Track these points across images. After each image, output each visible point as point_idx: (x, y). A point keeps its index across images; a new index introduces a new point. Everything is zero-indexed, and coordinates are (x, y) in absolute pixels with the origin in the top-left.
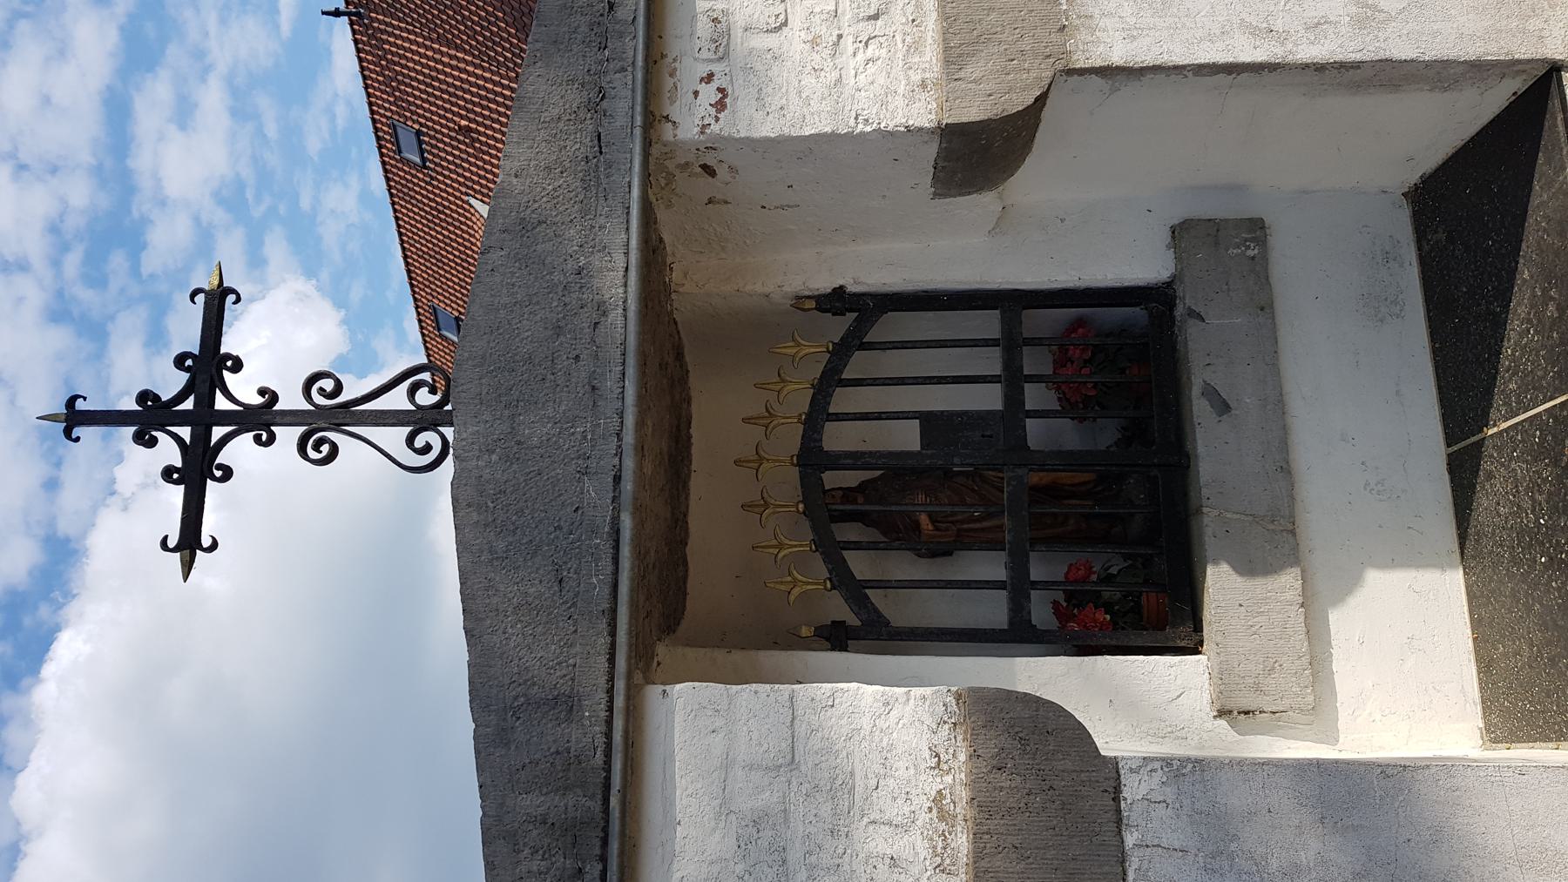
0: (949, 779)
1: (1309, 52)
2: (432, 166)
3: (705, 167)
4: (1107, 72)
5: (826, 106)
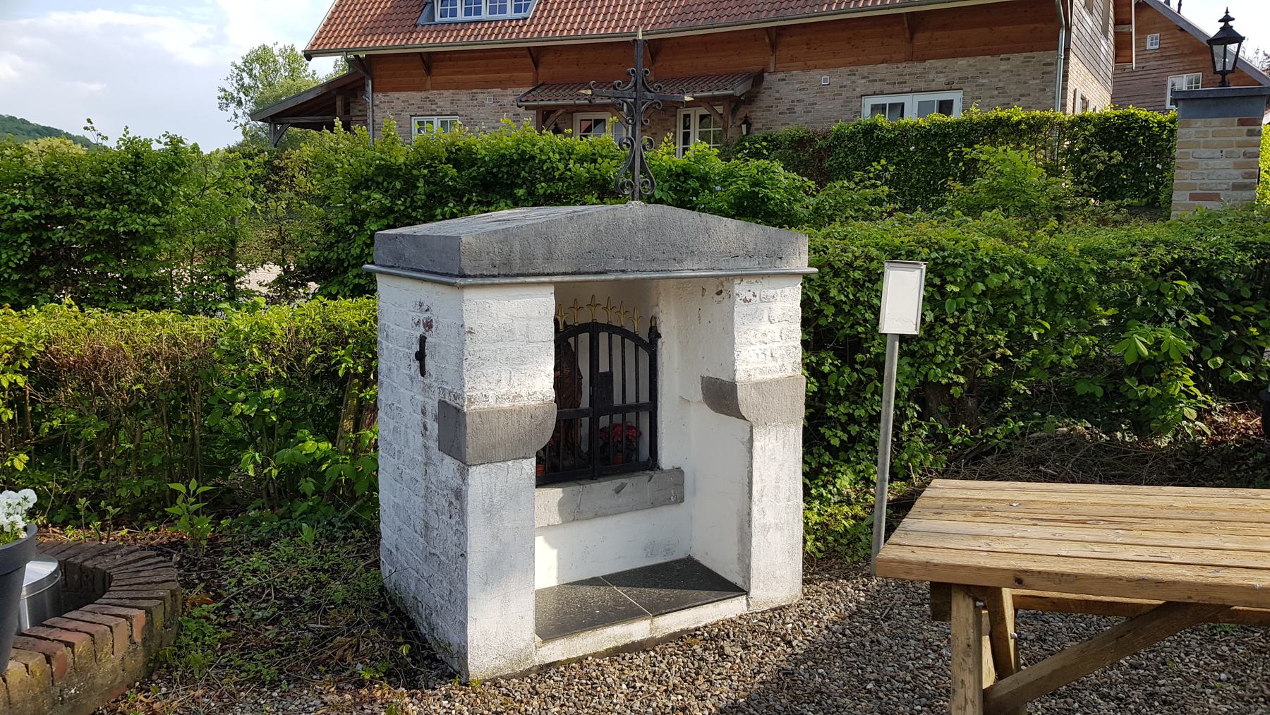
1: (755, 509)
3: (721, 292)
4: (751, 440)
5: (744, 341)
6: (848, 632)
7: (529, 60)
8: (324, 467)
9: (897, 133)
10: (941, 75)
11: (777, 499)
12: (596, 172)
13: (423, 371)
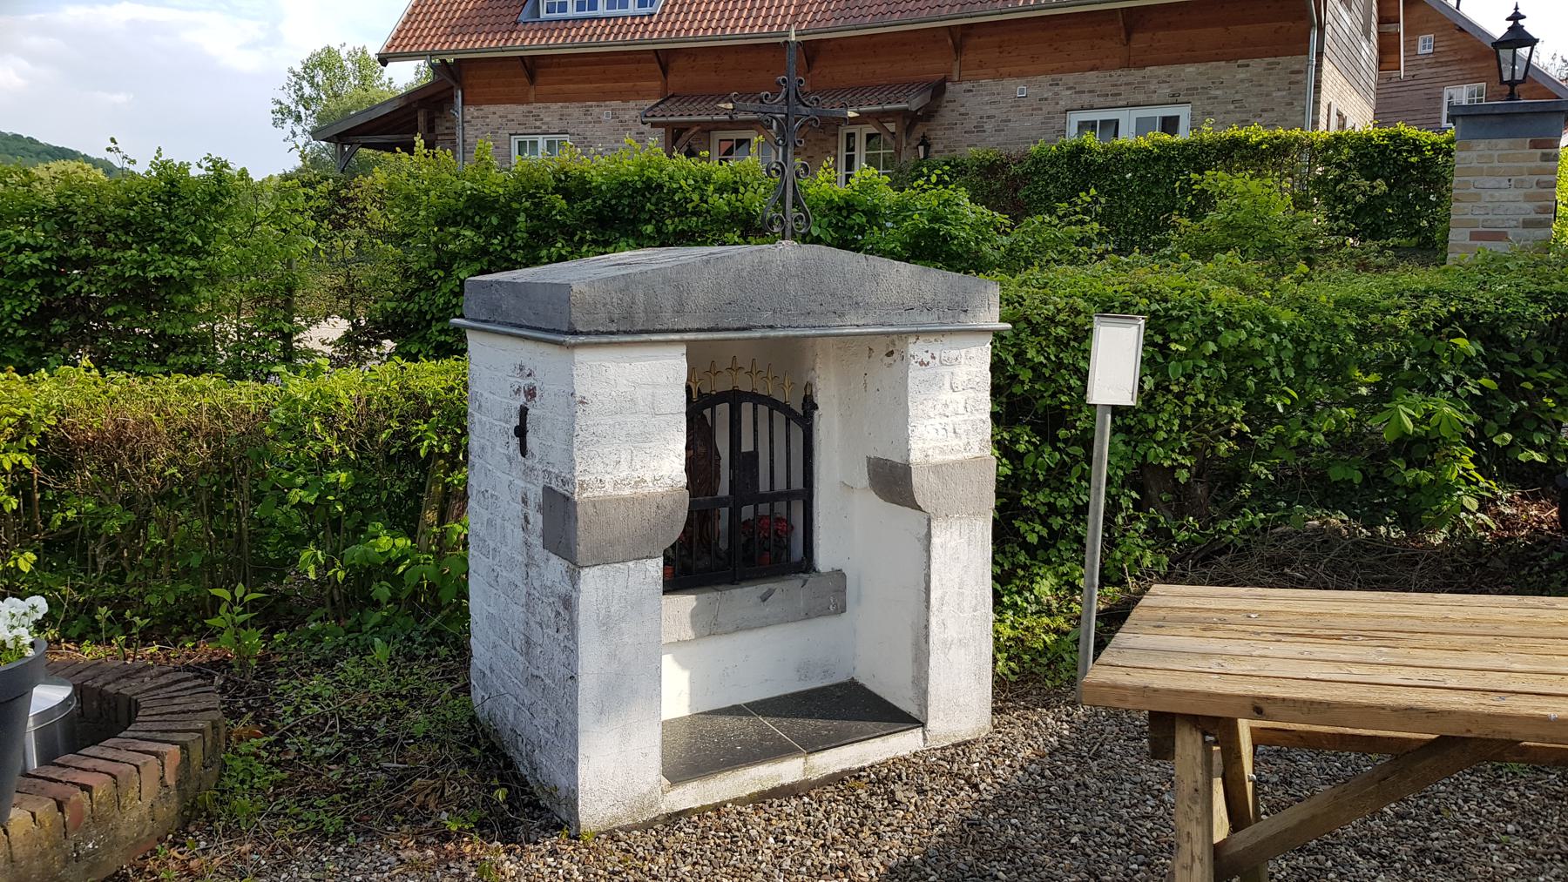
3: (892, 352)
4: (929, 536)
6: (1047, 773)
8: (401, 569)
9: (1110, 156)
11: (960, 609)
13: (523, 450)
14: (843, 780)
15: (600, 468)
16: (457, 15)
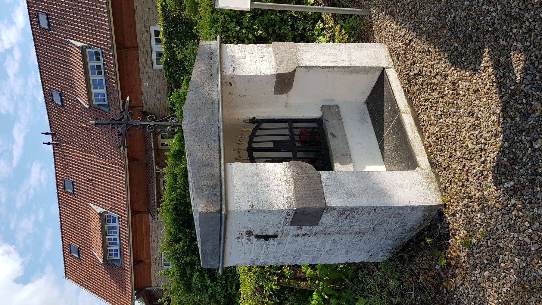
0: (288, 177)
1: (341, 65)
2: (77, 193)
3: (230, 83)
4: (306, 67)
5: (255, 70)
6: (402, 13)
7: (137, 215)
8: (326, 297)
9: (168, 52)
10: (144, 35)
11: (336, 55)
12: (181, 174)
13: (275, 236)
14: (410, 98)
15: (281, 198)
16: (119, 290)
